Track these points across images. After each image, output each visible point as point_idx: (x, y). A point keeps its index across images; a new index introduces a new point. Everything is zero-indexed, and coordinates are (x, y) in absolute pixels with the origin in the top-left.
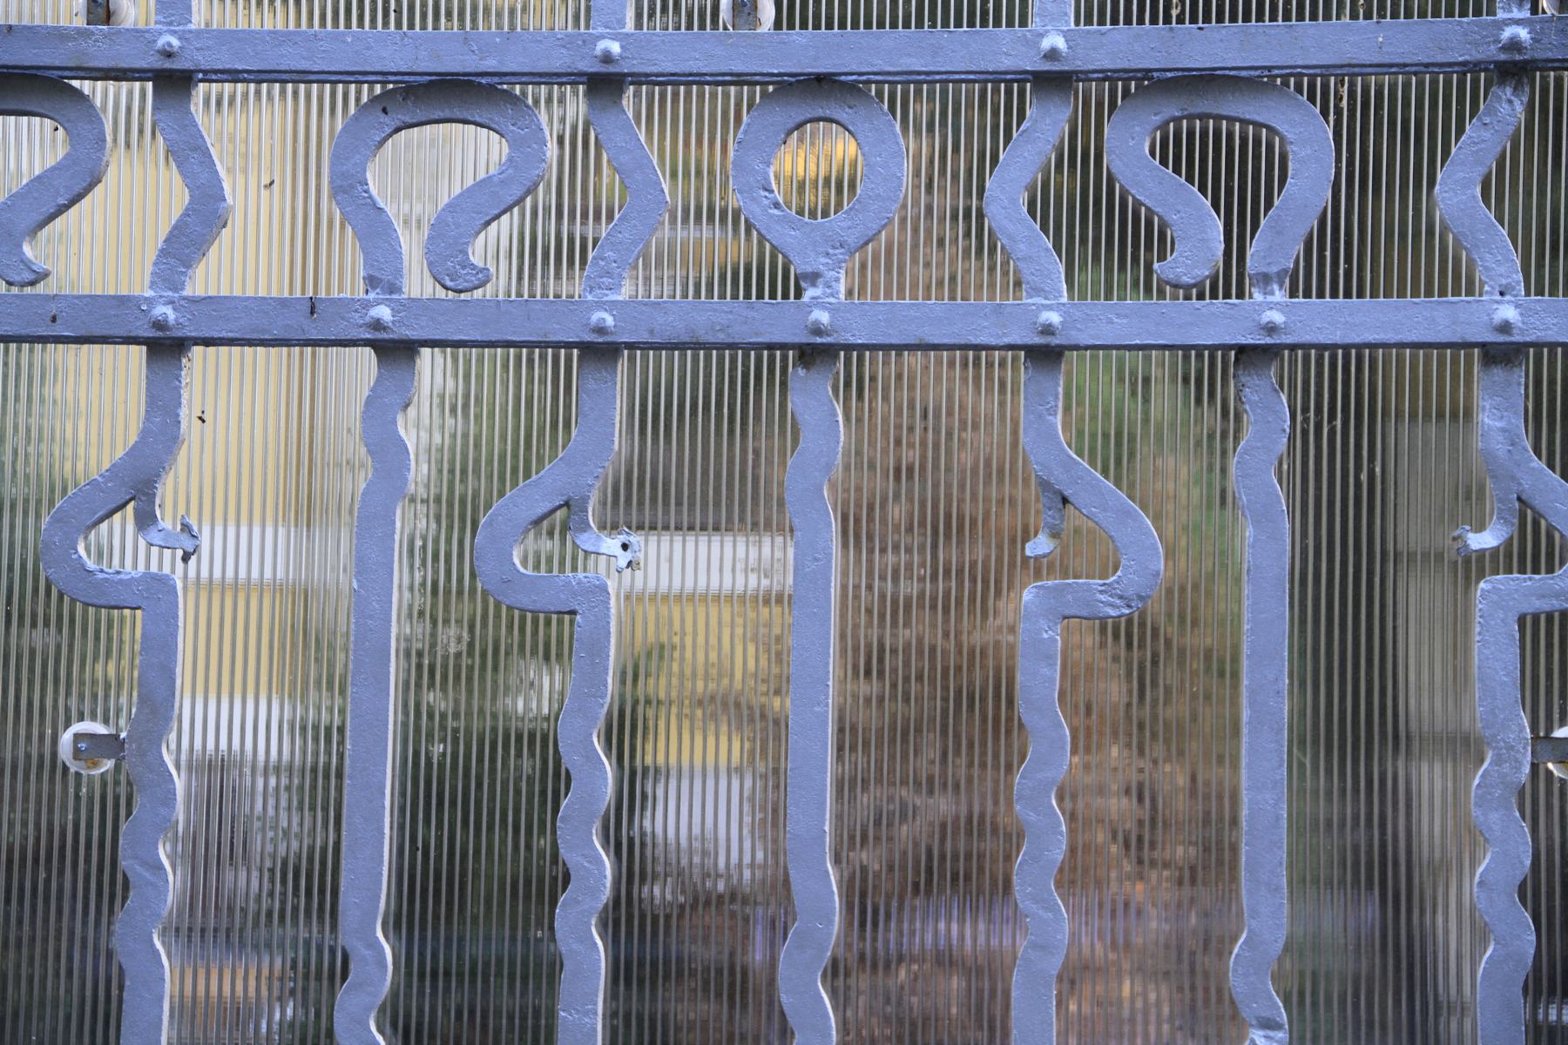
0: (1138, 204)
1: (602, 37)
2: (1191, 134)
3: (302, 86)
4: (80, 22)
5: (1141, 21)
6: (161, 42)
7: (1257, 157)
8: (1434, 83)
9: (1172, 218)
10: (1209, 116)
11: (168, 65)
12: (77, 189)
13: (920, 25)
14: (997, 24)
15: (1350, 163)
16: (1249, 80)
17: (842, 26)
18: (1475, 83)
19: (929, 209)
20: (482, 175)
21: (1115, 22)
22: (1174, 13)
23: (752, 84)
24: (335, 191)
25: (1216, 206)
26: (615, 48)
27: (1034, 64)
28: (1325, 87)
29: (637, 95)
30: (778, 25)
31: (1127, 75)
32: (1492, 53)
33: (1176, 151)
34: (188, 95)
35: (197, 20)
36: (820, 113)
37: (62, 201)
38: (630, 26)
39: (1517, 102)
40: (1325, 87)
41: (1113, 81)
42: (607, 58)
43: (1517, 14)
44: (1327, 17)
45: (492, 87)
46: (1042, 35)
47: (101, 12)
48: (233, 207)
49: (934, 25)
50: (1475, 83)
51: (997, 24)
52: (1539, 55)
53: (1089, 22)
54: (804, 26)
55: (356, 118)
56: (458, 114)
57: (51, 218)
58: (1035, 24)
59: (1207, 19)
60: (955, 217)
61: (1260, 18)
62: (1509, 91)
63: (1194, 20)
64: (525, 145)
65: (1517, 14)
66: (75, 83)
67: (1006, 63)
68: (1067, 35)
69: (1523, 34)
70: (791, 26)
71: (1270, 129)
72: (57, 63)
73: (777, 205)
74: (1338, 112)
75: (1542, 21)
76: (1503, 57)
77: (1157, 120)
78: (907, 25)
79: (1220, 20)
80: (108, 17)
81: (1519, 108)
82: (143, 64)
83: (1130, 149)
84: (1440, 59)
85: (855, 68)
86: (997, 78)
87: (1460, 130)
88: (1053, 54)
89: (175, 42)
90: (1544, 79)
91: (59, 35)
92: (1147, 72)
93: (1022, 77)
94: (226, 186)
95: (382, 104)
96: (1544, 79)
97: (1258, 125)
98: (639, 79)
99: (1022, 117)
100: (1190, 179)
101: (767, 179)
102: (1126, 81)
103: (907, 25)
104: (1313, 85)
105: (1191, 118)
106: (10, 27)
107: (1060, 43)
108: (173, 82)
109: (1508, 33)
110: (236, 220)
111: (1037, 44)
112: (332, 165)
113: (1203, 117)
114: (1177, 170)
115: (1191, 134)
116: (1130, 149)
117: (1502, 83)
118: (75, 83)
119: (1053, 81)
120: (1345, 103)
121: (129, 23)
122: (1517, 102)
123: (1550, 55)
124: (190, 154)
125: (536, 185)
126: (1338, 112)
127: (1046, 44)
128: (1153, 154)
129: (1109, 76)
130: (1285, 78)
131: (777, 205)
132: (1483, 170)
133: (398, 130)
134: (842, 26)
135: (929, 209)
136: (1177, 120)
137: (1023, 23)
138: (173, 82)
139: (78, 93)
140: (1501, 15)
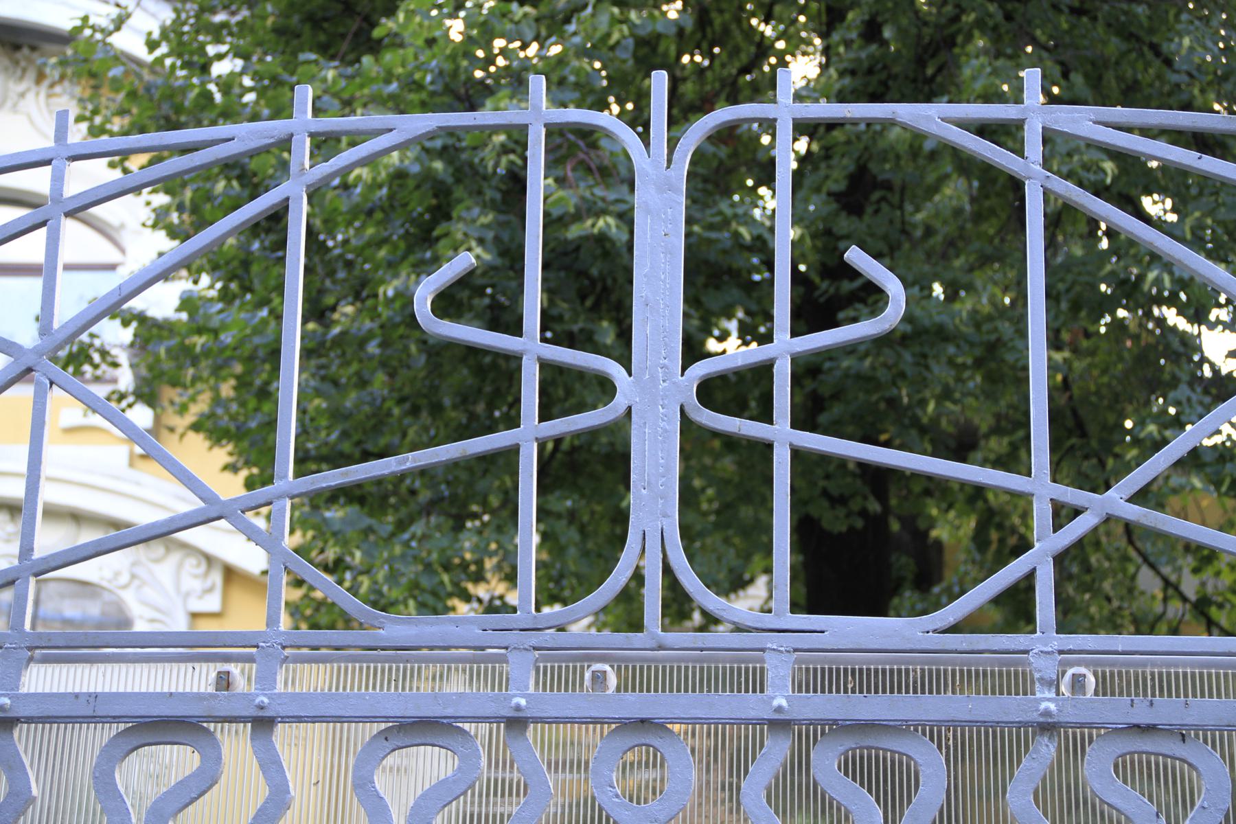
0: (831, 799)
1: (515, 696)
2: (862, 758)
3: (338, 725)
4: (211, 690)
5: (830, 691)
6: (257, 701)
7: (901, 773)
8: (1002, 733)
9: (852, 808)
10: (872, 748)
11: (261, 714)
12: (204, 788)
13: (701, 690)
14: (747, 691)
15: (956, 778)
16: (894, 727)
17: (656, 690)
18: (1026, 733)
19: (708, 783)
20: (442, 777)
21: (815, 691)
22: (850, 686)
23: (602, 723)
24: (356, 786)
25: (878, 801)
26: (523, 702)
27: (769, 715)
28: (939, 732)
29: (535, 730)
30: (618, 689)
31: (823, 722)
32: (1035, 717)
33: (853, 767)
34: (272, 731)
35: (280, 688)
36: (643, 741)
37: (194, 795)
38: (531, 689)
39: (1051, 746)
40: (939, 732)
41: (815, 726)
42: (518, 708)
43: (1047, 695)
44: (938, 692)
45: (450, 724)
46: (773, 698)
47: (225, 683)
48: (293, 798)
49: (709, 691)
50: (1026, 733)
51: (747, 691)
52: (1061, 719)
53: (800, 691)
54: (634, 690)
55: (369, 743)
56: (429, 740)
57: (187, 806)
58: (769, 691)
59: (869, 691)
60: (723, 788)
61: (899, 692)
62: (1046, 739)
63: (861, 692)
64: (467, 760)
65: (1047, 695)
66: (205, 725)
67: (752, 714)
68: (787, 698)
69: (1052, 707)
70: (626, 690)
71: (908, 756)
72: (197, 714)
73: (617, 796)
74: (948, 747)
75: (1063, 700)
76: (1041, 720)
77: (842, 749)
78: (694, 691)
79: (876, 692)
80: (228, 686)
81: (1053, 750)
82: (247, 714)
83: (826, 764)
84: (1005, 719)
85: (663, 715)
86: (747, 722)
87: (1019, 762)
88: (779, 709)
89: (266, 700)
90: (1066, 733)
91: (199, 697)
92: (835, 721)
93: (761, 722)
94: (291, 785)
95: (385, 735)
96: (1066, 733)
97: (901, 754)
98: (536, 720)
99: (762, 746)
100: (862, 784)
101: (611, 780)
102: (823, 725)
103: (694, 691)
104: (933, 731)
105: (861, 748)
106: (171, 694)
107: (784, 703)
108: (263, 724)
109: (1043, 706)
110: (296, 805)
111: (771, 703)
112: (354, 772)
113: (869, 748)
114: (854, 779)
115: (862, 758)
116: (826, 764)
117: (1041, 735)
118: (205, 725)
119: (779, 725)
120: (951, 742)
121: (239, 690)
122: (1051, 746)
123: (1068, 720)
124: (271, 765)
125: (474, 783)
126: (948, 747)
127: (776, 703)
128: (839, 769)
129: (812, 722)
130: (916, 727)
131: (617, 796)
132: (1033, 786)
133: (394, 750)
134: (656, 690)
135: (708, 783)
136: (854, 750)
137: (762, 691)
138: (263, 724)
139: (207, 730)
140: (1038, 695)
